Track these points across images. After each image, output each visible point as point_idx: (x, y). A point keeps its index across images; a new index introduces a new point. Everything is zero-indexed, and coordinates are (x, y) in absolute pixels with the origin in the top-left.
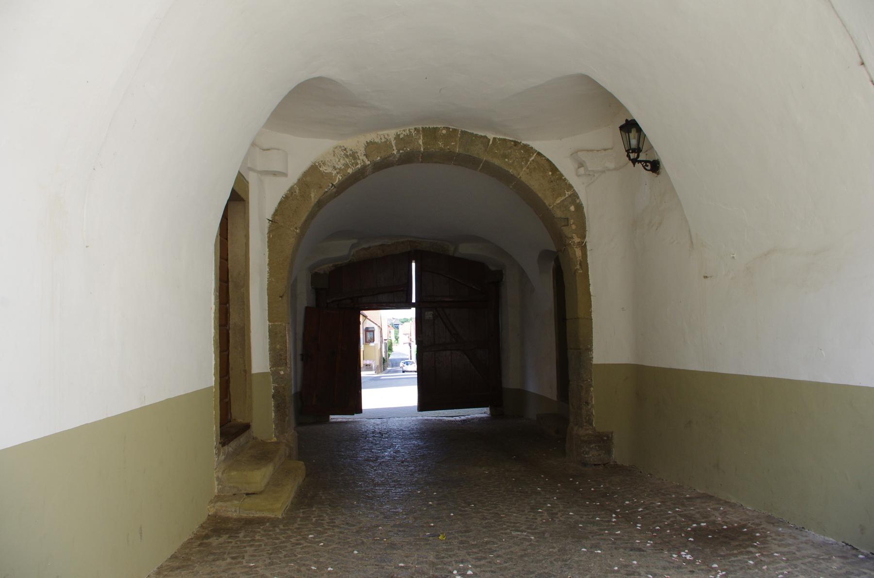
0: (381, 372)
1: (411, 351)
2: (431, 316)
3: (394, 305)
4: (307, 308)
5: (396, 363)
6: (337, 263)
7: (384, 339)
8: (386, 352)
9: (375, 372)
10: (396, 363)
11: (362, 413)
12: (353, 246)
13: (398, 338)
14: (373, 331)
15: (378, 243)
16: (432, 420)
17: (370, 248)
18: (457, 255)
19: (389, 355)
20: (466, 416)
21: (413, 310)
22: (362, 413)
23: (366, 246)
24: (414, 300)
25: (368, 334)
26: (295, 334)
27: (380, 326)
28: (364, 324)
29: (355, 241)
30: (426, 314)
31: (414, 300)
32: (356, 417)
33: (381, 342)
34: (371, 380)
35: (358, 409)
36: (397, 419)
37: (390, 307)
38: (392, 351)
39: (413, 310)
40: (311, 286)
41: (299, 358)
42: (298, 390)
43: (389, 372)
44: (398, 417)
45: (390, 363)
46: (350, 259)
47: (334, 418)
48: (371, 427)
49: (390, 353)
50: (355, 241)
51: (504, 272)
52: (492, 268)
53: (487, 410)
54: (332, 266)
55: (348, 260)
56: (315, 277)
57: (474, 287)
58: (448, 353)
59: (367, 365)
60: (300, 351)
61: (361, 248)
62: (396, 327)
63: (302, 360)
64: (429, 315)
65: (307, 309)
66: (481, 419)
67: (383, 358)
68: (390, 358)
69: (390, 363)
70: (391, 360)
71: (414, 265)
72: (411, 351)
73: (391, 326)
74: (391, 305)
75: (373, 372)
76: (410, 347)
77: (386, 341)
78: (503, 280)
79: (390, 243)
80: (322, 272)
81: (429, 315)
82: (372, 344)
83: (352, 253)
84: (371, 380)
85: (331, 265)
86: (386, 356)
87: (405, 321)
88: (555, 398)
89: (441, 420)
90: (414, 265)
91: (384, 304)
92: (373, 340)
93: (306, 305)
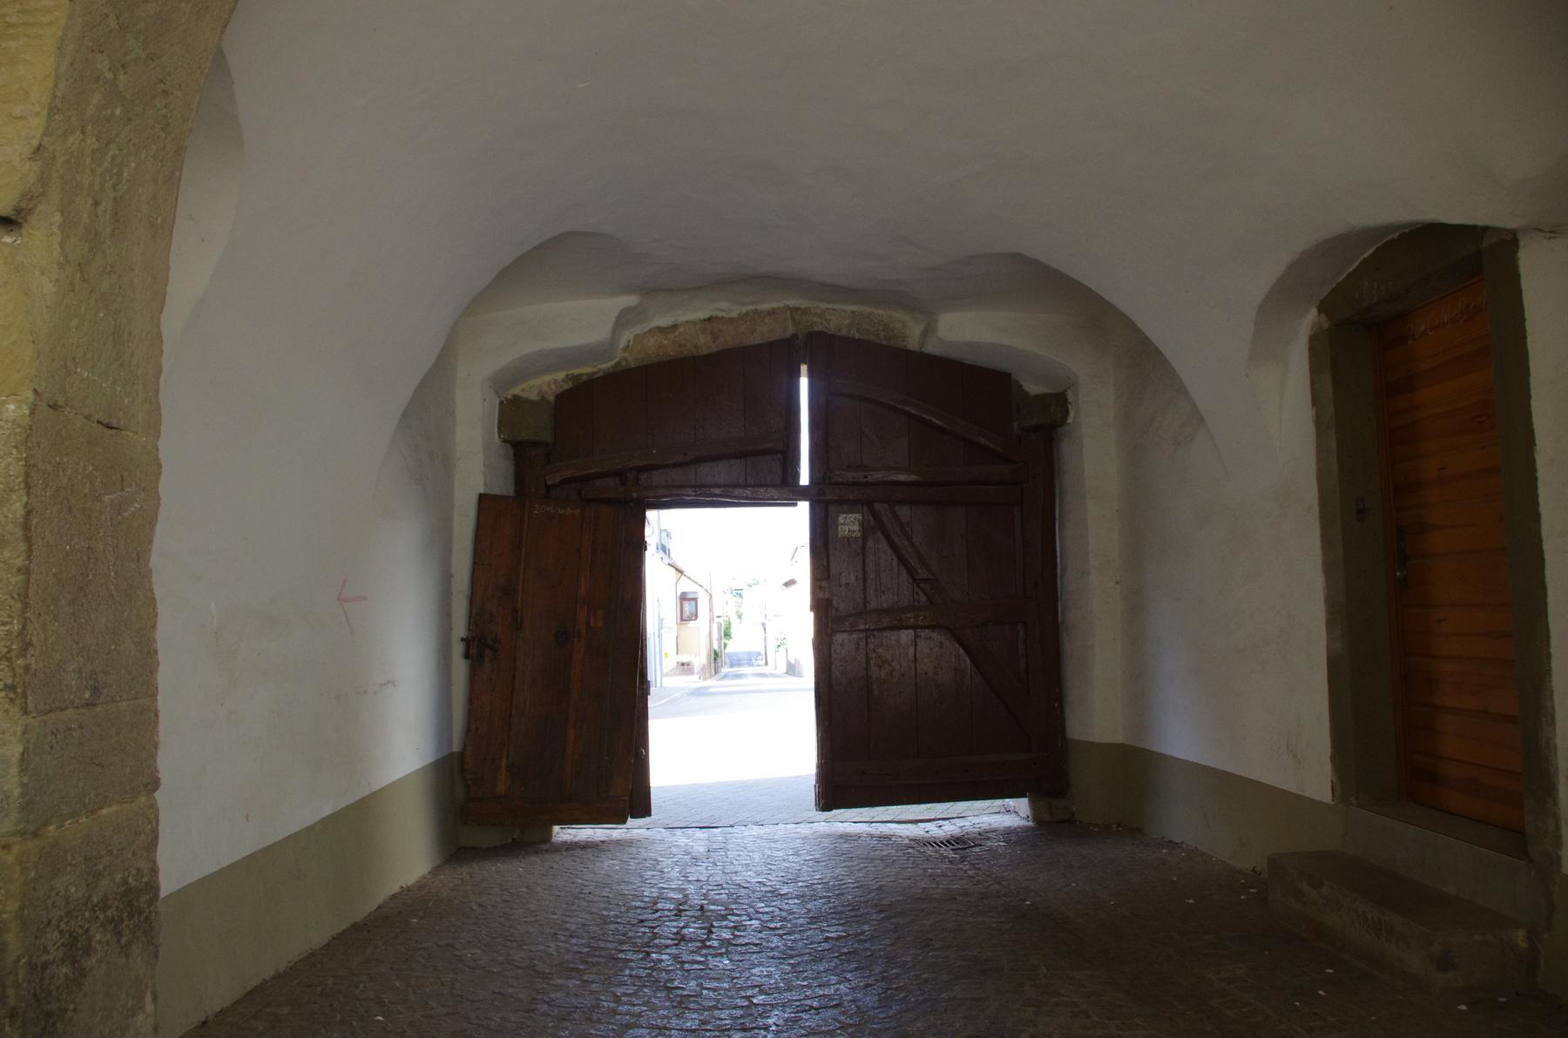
0: (711, 676)
1: (765, 637)
2: (856, 527)
3: (748, 492)
4: (482, 498)
5: (736, 662)
6: (577, 371)
7: (715, 615)
8: (720, 639)
9: (700, 678)
10: (739, 660)
11: (650, 815)
12: (624, 319)
13: (742, 614)
14: (695, 600)
15: (699, 311)
16: (859, 836)
17: (675, 327)
18: (931, 348)
19: (725, 645)
20: (960, 823)
21: (804, 507)
22: (650, 815)
23: (664, 321)
24: (805, 479)
25: (686, 604)
26: (446, 577)
27: (708, 589)
28: (651, 535)
29: (631, 300)
30: (841, 519)
31: (805, 479)
32: (634, 828)
33: (711, 621)
34: (690, 694)
35: (637, 802)
36: (756, 831)
37: (734, 497)
38: (731, 638)
39: (804, 507)
40: (499, 432)
41: (458, 649)
42: (456, 748)
43: (726, 676)
44: (756, 824)
45: (727, 661)
46: (617, 360)
47: (563, 834)
48: (674, 874)
49: (727, 642)
50: (631, 300)
51: (1070, 398)
52: (1033, 388)
53: (1022, 805)
54: (563, 381)
55: (612, 363)
56: (512, 412)
57: (982, 441)
58: (906, 636)
59: (683, 664)
60: (460, 629)
61: (647, 326)
62: (738, 593)
63: (467, 656)
64: (849, 524)
65: (485, 502)
66: (1008, 833)
67: (715, 651)
68: (726, 651)
69: (727, 661)
70: (729, 655)
71: (804, 383)
72: (765, 637)
73: (728, 592)
74: (737, 492)
75: (696, 677)
76: (765, 630)
77: (721, 620)
78: (1070, 420)
79: (734, 315)
80: (534, 396)
81: (849, 524)
82: (692, 623)
83: (623, 343)
84: (690, 694)
85: (561, 375)
86: (720, 647)
87: (755, 584)
88: (1325, 796)
89: (888, 837)
90: (804, 383)
91: (718, 491)
92: (694, 616)
93: (482, 491)
